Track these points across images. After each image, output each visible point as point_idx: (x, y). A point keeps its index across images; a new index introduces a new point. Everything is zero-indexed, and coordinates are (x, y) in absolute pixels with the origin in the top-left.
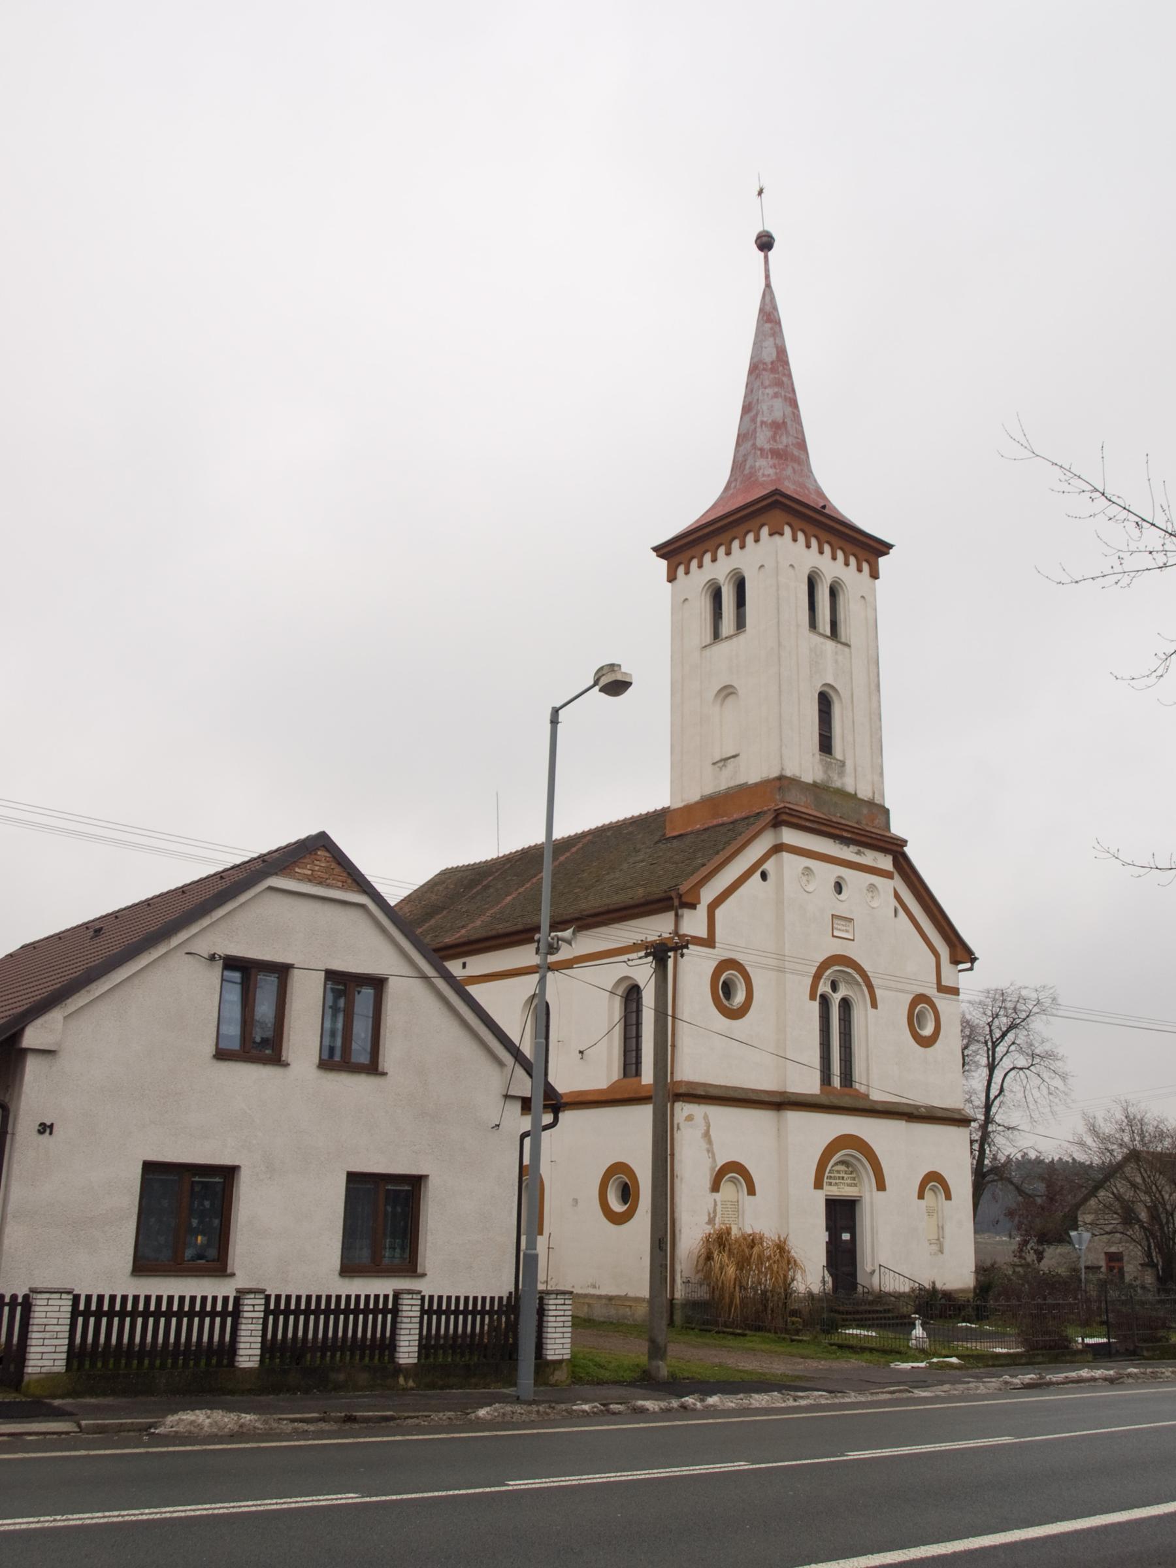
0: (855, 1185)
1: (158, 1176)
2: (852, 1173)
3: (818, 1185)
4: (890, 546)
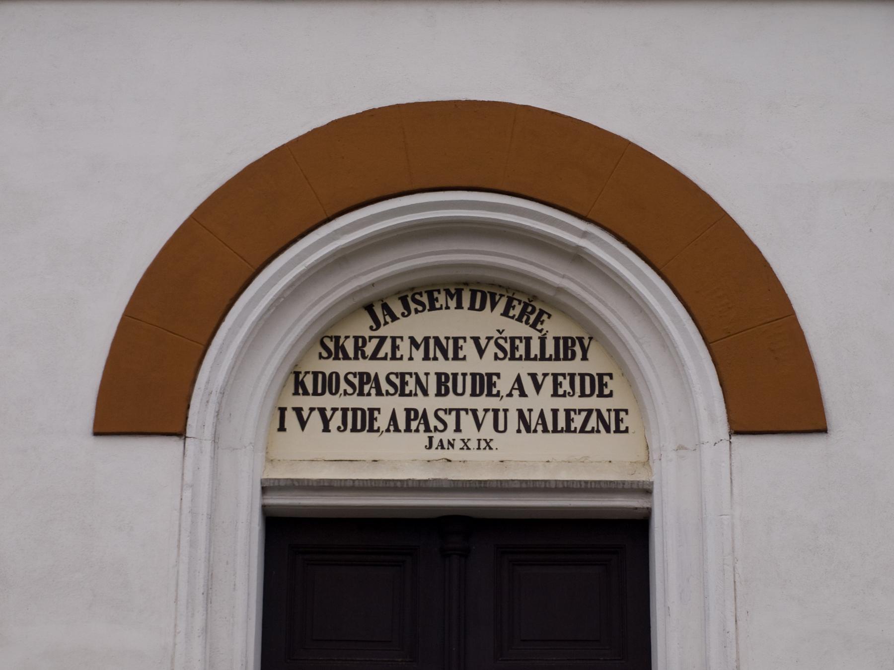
0: (614, 423)
1: (285, 430)
2: (566, 348)
3: (144, 391)
4: (529, 374)
